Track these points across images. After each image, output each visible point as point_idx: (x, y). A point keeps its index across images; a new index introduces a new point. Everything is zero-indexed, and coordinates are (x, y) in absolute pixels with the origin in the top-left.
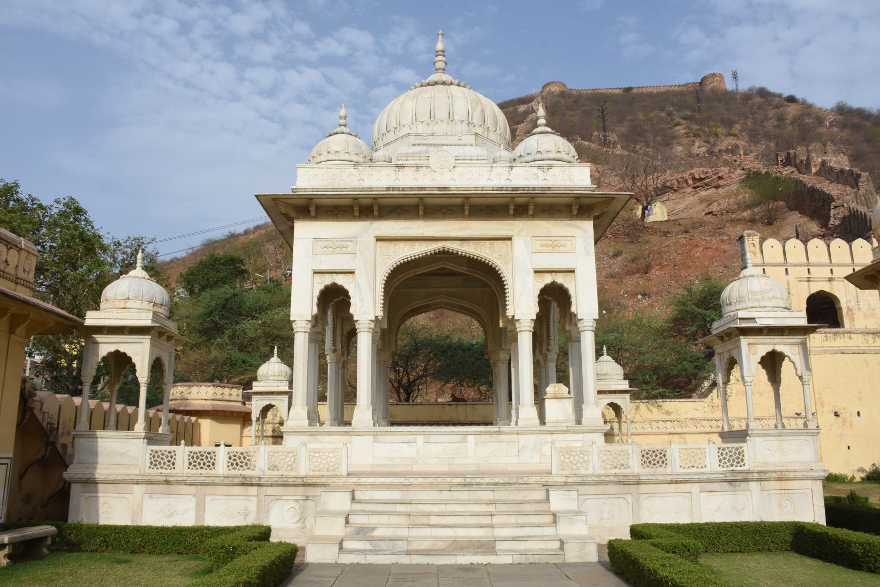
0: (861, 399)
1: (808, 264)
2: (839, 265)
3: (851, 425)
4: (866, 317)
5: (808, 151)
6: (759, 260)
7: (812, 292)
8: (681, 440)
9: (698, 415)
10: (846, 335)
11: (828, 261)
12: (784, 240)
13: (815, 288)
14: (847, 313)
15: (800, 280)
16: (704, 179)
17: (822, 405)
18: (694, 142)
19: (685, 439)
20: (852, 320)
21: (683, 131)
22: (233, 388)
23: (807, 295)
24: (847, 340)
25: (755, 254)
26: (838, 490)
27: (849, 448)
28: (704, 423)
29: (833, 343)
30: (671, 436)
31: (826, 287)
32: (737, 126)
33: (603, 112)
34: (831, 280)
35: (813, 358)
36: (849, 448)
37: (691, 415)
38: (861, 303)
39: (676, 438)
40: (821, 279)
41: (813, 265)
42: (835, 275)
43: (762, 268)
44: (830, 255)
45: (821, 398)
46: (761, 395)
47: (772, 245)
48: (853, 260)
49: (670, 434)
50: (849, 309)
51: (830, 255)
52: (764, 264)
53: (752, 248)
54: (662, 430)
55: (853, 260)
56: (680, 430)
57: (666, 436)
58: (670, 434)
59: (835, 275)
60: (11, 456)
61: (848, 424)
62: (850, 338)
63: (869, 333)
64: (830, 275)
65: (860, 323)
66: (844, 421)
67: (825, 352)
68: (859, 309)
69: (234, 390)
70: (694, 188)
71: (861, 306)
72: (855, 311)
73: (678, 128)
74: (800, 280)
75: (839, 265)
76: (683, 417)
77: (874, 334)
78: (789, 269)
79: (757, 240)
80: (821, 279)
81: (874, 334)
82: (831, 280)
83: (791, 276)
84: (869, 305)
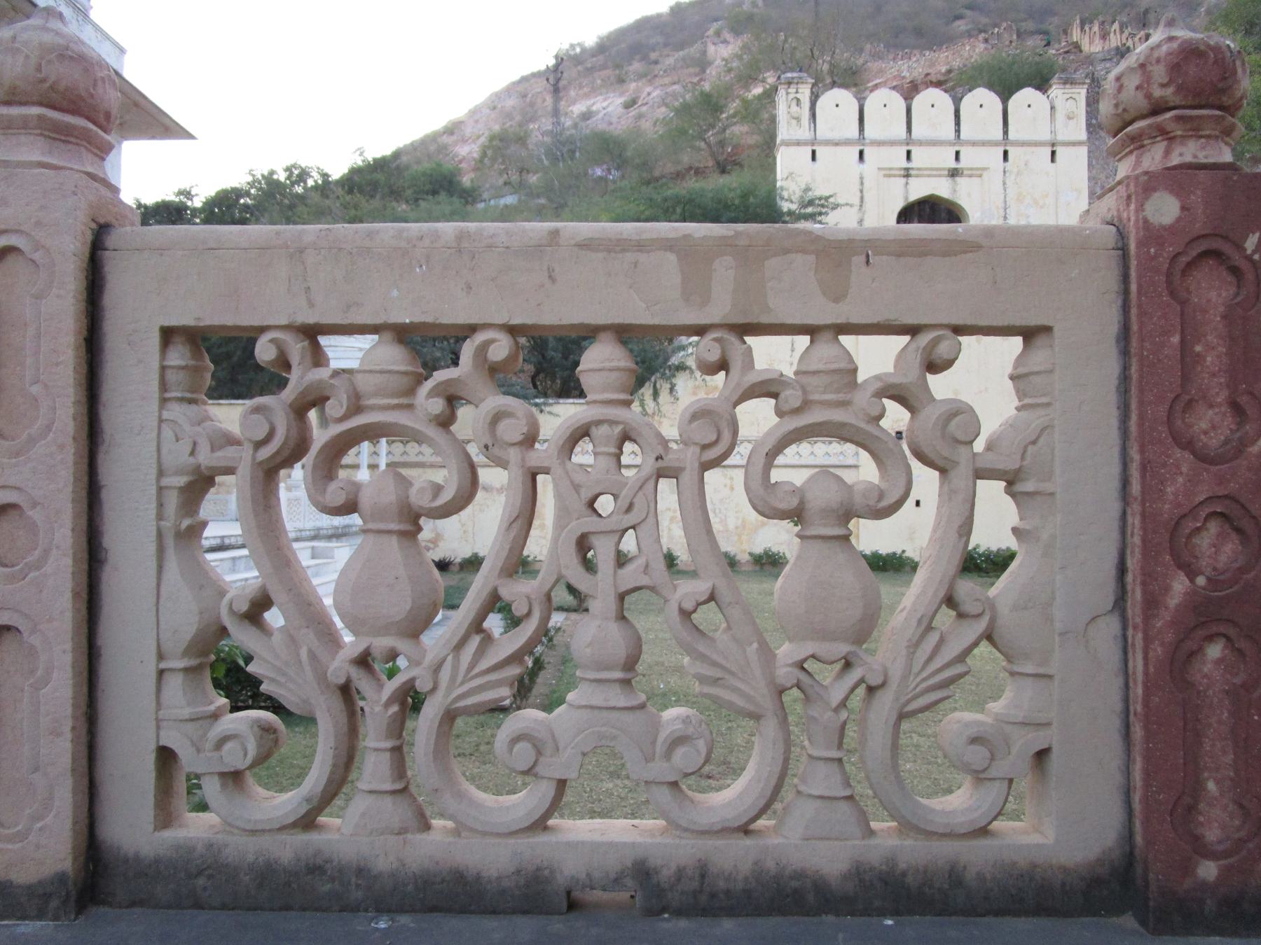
1: (909, 140)
2: (974, 144)
6: (804, 133)
15: (888, 173)
21: (963, 28)
22: (830, 443)
25: (798, 119)
26: (1133, 591)
32: (1056, 20)
34: (954, 173)
40: (933, 172)
41: (920, 143)
42: (963, 164)
43: (809, 150)
47: (838, 106)
48: (958, 131)
52: (813, 142)
53: (794, 108)
59: (963, 164)
60: (240, 532)
64: (953, 164)
69: (819, 444)
73: (958, 23)
74: (888, 173)
75: (974, 144)
79: (805, 92)
80: (933, 172)
82: (954, 173)
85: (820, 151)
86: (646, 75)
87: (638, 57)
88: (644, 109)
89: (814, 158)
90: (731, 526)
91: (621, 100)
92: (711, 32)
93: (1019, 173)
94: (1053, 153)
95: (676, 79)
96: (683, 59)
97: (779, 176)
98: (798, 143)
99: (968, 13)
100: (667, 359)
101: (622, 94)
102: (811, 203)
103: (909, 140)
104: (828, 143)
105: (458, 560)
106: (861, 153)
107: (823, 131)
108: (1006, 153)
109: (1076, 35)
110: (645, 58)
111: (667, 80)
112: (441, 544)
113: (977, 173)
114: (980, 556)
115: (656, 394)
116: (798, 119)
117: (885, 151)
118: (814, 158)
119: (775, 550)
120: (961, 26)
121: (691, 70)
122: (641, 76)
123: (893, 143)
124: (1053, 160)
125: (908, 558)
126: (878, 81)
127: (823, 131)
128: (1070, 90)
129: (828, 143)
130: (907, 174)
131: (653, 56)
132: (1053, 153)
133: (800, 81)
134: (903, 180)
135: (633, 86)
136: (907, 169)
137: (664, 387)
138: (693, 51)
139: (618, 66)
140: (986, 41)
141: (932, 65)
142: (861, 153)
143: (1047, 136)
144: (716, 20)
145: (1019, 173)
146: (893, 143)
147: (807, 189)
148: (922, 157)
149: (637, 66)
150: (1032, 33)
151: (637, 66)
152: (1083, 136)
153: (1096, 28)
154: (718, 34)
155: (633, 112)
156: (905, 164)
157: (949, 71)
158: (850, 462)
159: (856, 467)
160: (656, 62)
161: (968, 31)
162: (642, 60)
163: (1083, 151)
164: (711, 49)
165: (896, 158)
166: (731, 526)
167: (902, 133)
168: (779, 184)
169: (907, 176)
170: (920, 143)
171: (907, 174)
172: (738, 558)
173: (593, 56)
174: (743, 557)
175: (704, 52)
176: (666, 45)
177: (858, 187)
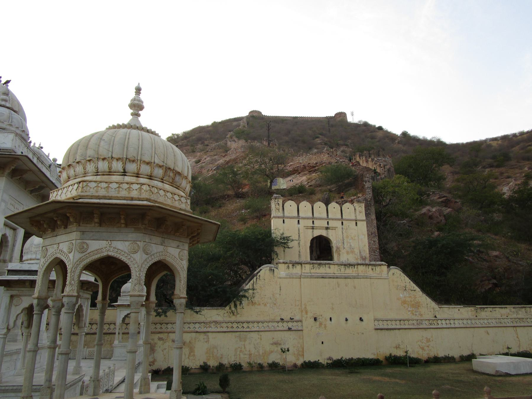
0: (333, 309)
1: (313, 217)
2: (333, 219)
3: (325, 327)
4: (348, 253)
5: (369, 154)
6: (280, 214)
7: (315, 236)
8: (205, 337)
9: (219, 319)
10: (327, 266)
11: (326, 216)
12: (312, 203)
13: (317, 233)
14: (336, 250)
15: (307, 228)
16: (315, 167)
17: (307, 313)
18: (324, 147)
19: (208, 336)
20: (339, 255)
21: (319, 142)
23: (311, 238)
24: (327, 269)
27: (322, 343)
28: (223, 325)
29: (318, 271)
30: (198, 334)
31: (324, 233)
32: (350, 141)
33: (269, 127)
34: (327, 228)
35: (296, 281)
36: (322, 343)
37: (214, 319)
38: (345, 244)
39: (202, 336)
40: (320, 228)
41: (317, 219)
42: (330, 226)
43: (282, 220)
44: (327, 213)
45: (306, 308)
46: (265, 305)
48: (328, 215)
49: (197, 332)
50: (338, 248)
51: (327, 213)
53: (277, 206)
54: (192, 329)
55: (328, 215)
56: (205, 330)
57: (195, 334)
58: (197, 332)
59: (330, 226)
61: (323, 326)
62: (330, 267)
63: (342, 265)
64: (327, 226)
65: (344, 257)
66: (321, 324)
67: (311, 277)
68: (344, 248)
70: (310, 172)
71: (345, 246)
72: (342, 249)
73: (317, 139)
75: (333, 219)
76: (209, 320)
77: (345, 265)
78: (300, 220)
81: (345, 265)
82: (327, 228)
83: (301, 226)
84: (351, 245)
85: (286, 220)
86: (203, 150)
87: (200, 142)
88: (204, 164)
89: (284, 222)
90: (261, 353)
91: (194, 160)
92: (228, 136)
93: (346, 229)
94: (356, 223)
95: (216, 154)
96: (218, 146)
97: (272, 228)
98: (279, 217)
99: (321, 136)
100: (239, 293)
101: (194, 157)
102: (284, 238)
103: (313, 217)
104: (288, 218)
105: (163, 369)
106: (298, 221)
107: (286, 214)
108: (342, 222)
109: (358, 159)
110: (203, 143)
111: (212, 153)
112: (156, 363)
113: (334, 228)
114: (344, 361)
115: (236, 306)
116: (279, 210)
117: (306, 221)
118: (284, 222)
119: (276, 361)
120: (318, 141)
121: (221, 150)
122: (202, 150)
123: (308, 218)
124: (356, 225)
125: (320, 363)
126: (291, 163)
127: (286, 214)
128: (359, 204)
129: (288, 218)
130: (313, 228)
131: (206, 143)
132: (356, 223)
133: (279, 198)
134: (312, 230)
135: (198, 154)
136: (313, 227)
137: (238, 303)
138: (222, 143)
139: (192, 146)
140: (328, 154)
141: (310, 160)
142: (298, 221)
143: (354, 218)
144: (230, 131)
145: (346, 229)
146: (308, 218)
147: (283, 234)
148: (317, 223)
149: (200, 146)
150: (342, 145)
151: (200, 146)
152: (364, 218)
153: (364, 159)
154: (231, 137)
155: (199, 165)
156: (312, 225)
157: (316, 163)
158: (300, 329)
159: (302, 330)
160: (207, 145)
161: (320, 143)
162: (202, 144)
163: (365, 223)
164: (229, 143)
165: (309, 223)
166: (261, 353)
167: (311, 215)
168: (272, 231)
169: (313, 229)
170: (317, 219)
171: (313, 228)
172: (264, 365)
173: (182, 140)
174: (265, 365)
175: (226, 144)
176: (211, 138)
177: (298, 232)
